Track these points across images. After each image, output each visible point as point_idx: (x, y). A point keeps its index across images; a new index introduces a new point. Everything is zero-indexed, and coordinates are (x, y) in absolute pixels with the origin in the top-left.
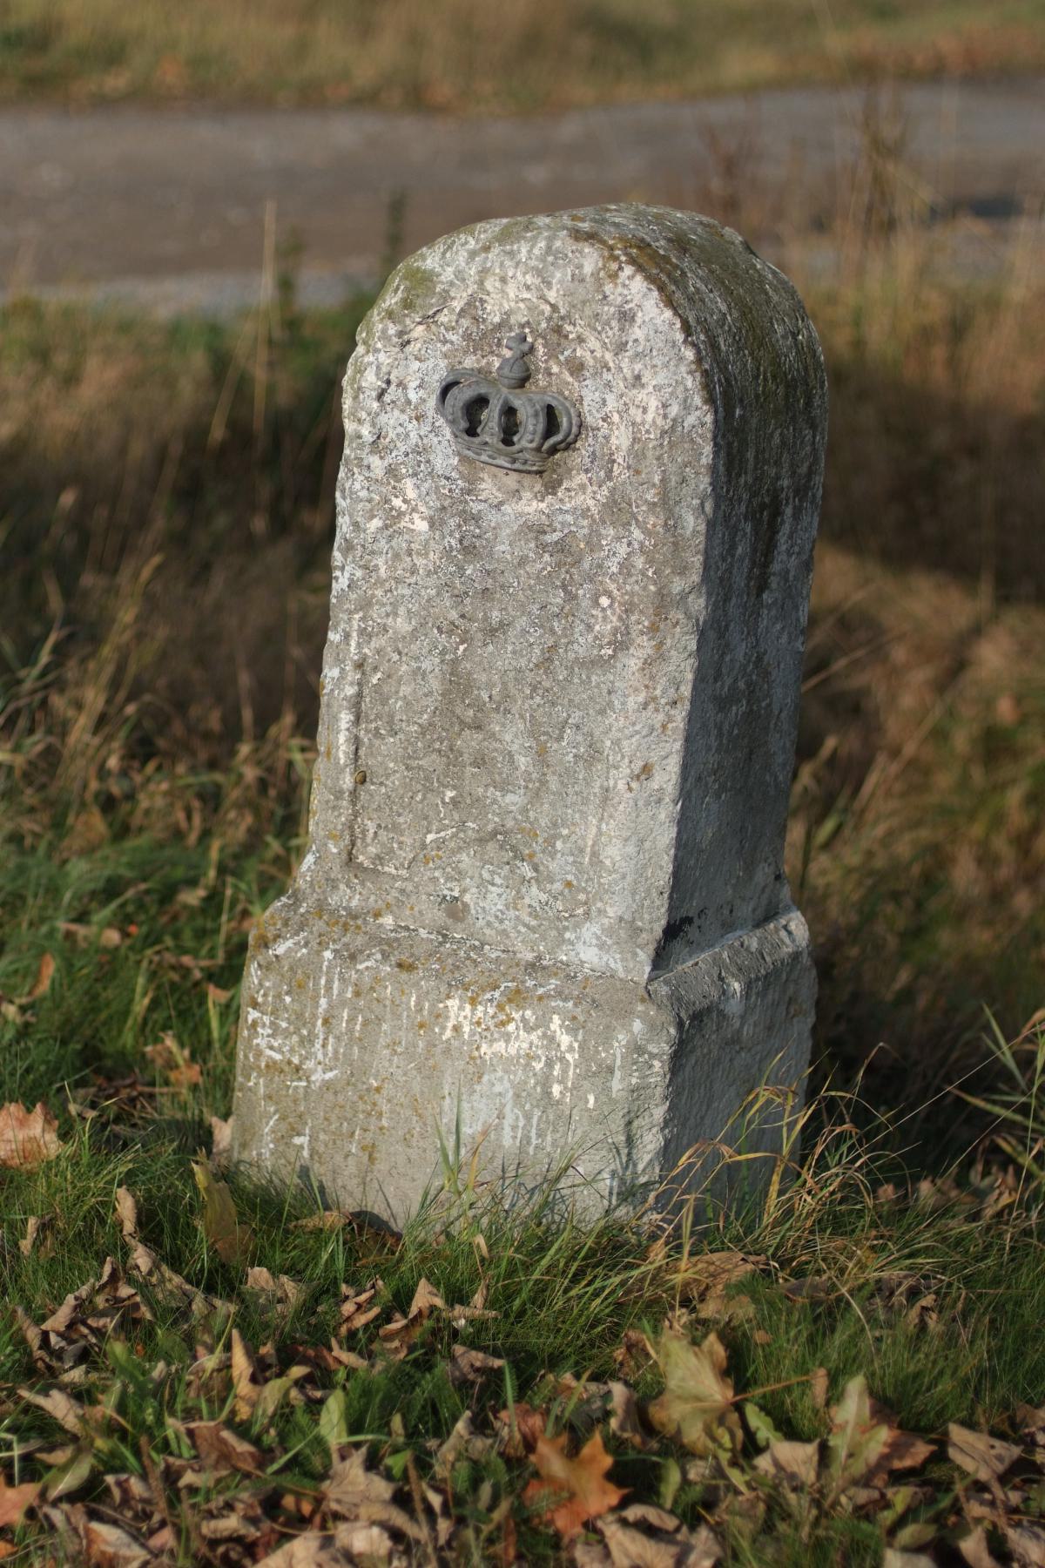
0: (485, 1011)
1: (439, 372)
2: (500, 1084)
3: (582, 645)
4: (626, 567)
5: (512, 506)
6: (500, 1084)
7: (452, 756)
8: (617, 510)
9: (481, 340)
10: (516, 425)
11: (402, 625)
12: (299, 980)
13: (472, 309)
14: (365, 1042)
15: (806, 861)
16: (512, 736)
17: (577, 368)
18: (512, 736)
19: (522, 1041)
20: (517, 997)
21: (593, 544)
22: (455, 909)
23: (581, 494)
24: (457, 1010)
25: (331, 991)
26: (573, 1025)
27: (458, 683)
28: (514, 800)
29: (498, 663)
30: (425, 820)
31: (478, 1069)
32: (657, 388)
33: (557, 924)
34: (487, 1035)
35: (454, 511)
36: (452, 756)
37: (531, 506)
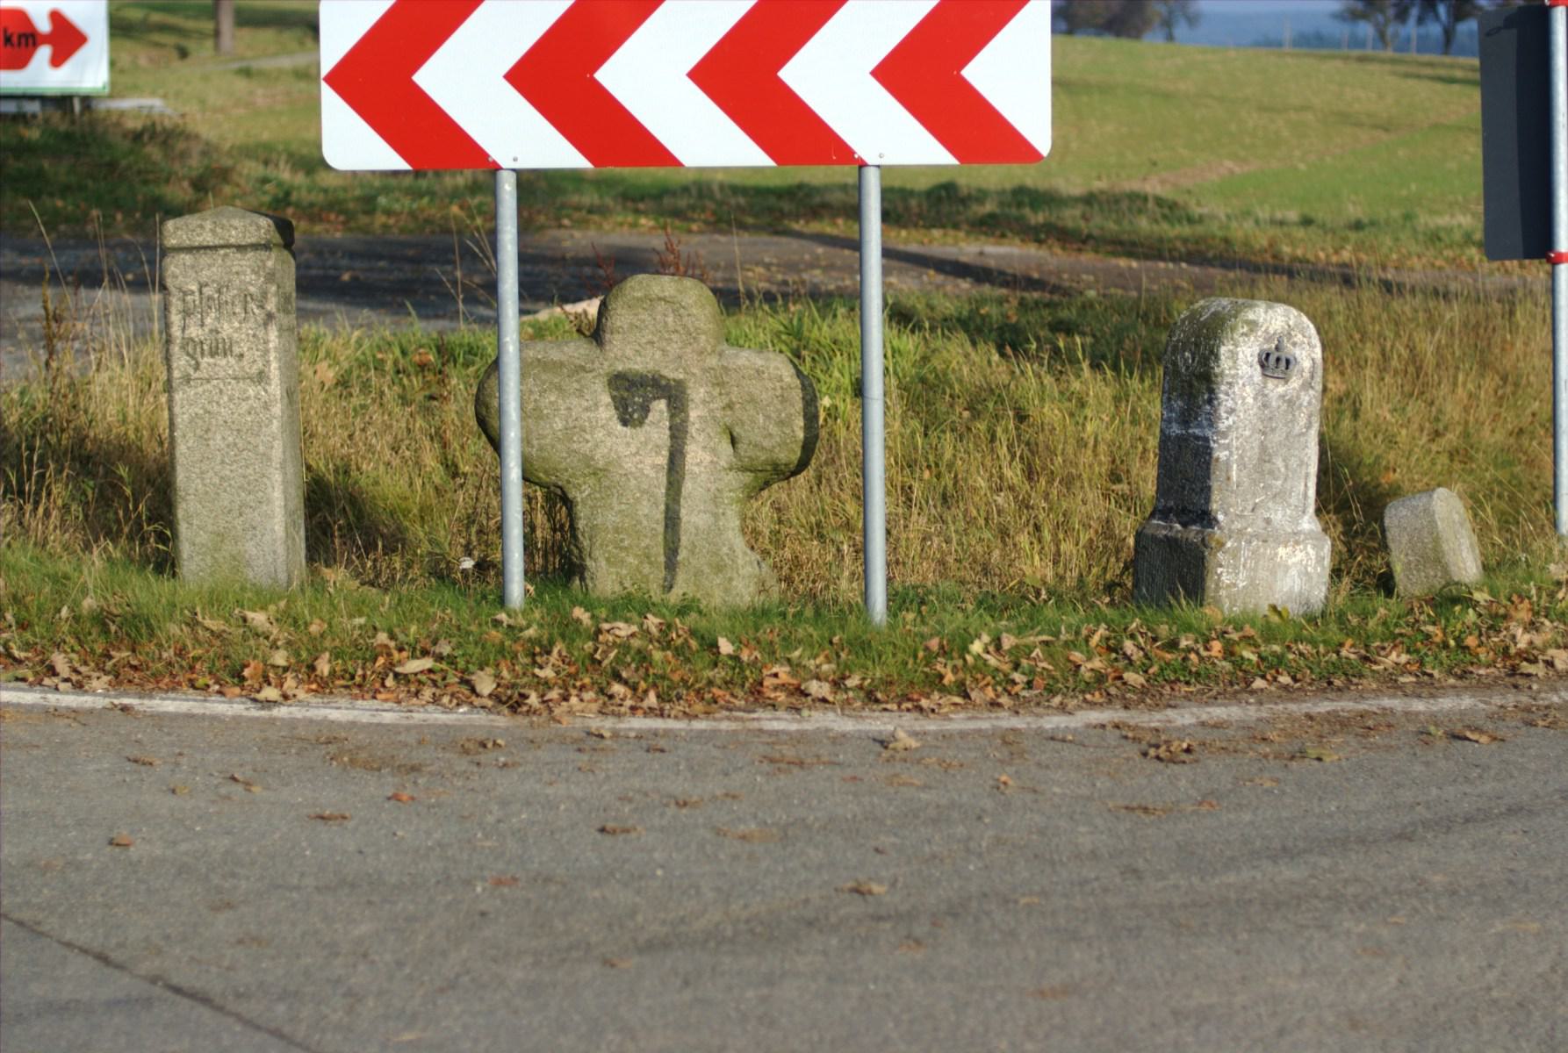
0: (1290, 549)
1: (1256, 350)
2: (1293, 572)
3: (1297, 430)
4: (1310, 403)
5: (1276, 389)
6: (1293, 572)
7: (1262, 473)
8: (1307, 386)
9: (1268, 340)
10: (653, 379)
11: (1247, 433)
12: (1235, 554)
13: (1266, 331)
14: (1255, 570)
15: (1058, 546)
16: (1280, 463)
17: (1294, 344)
18: (1280, 463)
19: (1300, 556)
20: (1297, 543)
21: (1298, 397)
22: (1268, 521)
23: (1295, 383)
24: (1282, 551)
25: (1245, 553)
26: (1314, 547)
27: (1263, 448)
28: (1279, 483)
29: (1277, 437)
30: (1255, 495)
31: (1287, 568)
32: (250, 349)
33: (1295, 521)
34: (1289, 557)
35: (1261, 394)
36: (1262, 473)
37: (1281, 389)
